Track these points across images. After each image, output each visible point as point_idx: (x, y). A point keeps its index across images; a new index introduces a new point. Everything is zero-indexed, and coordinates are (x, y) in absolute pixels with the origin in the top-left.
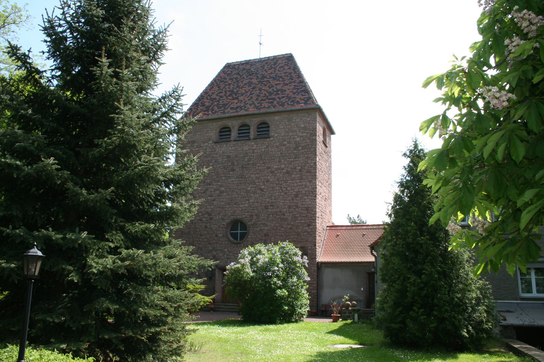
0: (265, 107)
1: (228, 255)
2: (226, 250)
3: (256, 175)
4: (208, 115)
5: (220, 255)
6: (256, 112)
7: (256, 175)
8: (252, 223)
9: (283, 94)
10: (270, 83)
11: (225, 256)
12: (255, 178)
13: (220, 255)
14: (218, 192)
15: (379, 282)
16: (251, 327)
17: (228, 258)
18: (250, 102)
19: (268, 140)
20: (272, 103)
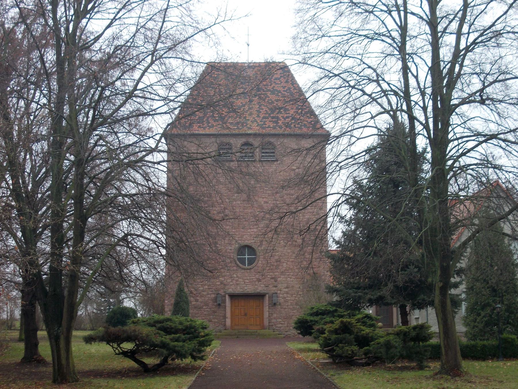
0: (269, 127)
1: (237, 281)
2: (235, 276)
3: (265, 199)
4: (204, 128)
5: (229, 281)
6: (272, 140)
7: (265, 199)
8: (262, 248)
9: (287, 114)
10: (269, 97)
11: (234, 281)
12: (262, 203)
13: (229, 281)
14: (223, 215)
15: (126, 328)
16: (158, 378)
17: (238, 284)
18: (251, 119)
19: (275, 163)
20: (277, 122)
